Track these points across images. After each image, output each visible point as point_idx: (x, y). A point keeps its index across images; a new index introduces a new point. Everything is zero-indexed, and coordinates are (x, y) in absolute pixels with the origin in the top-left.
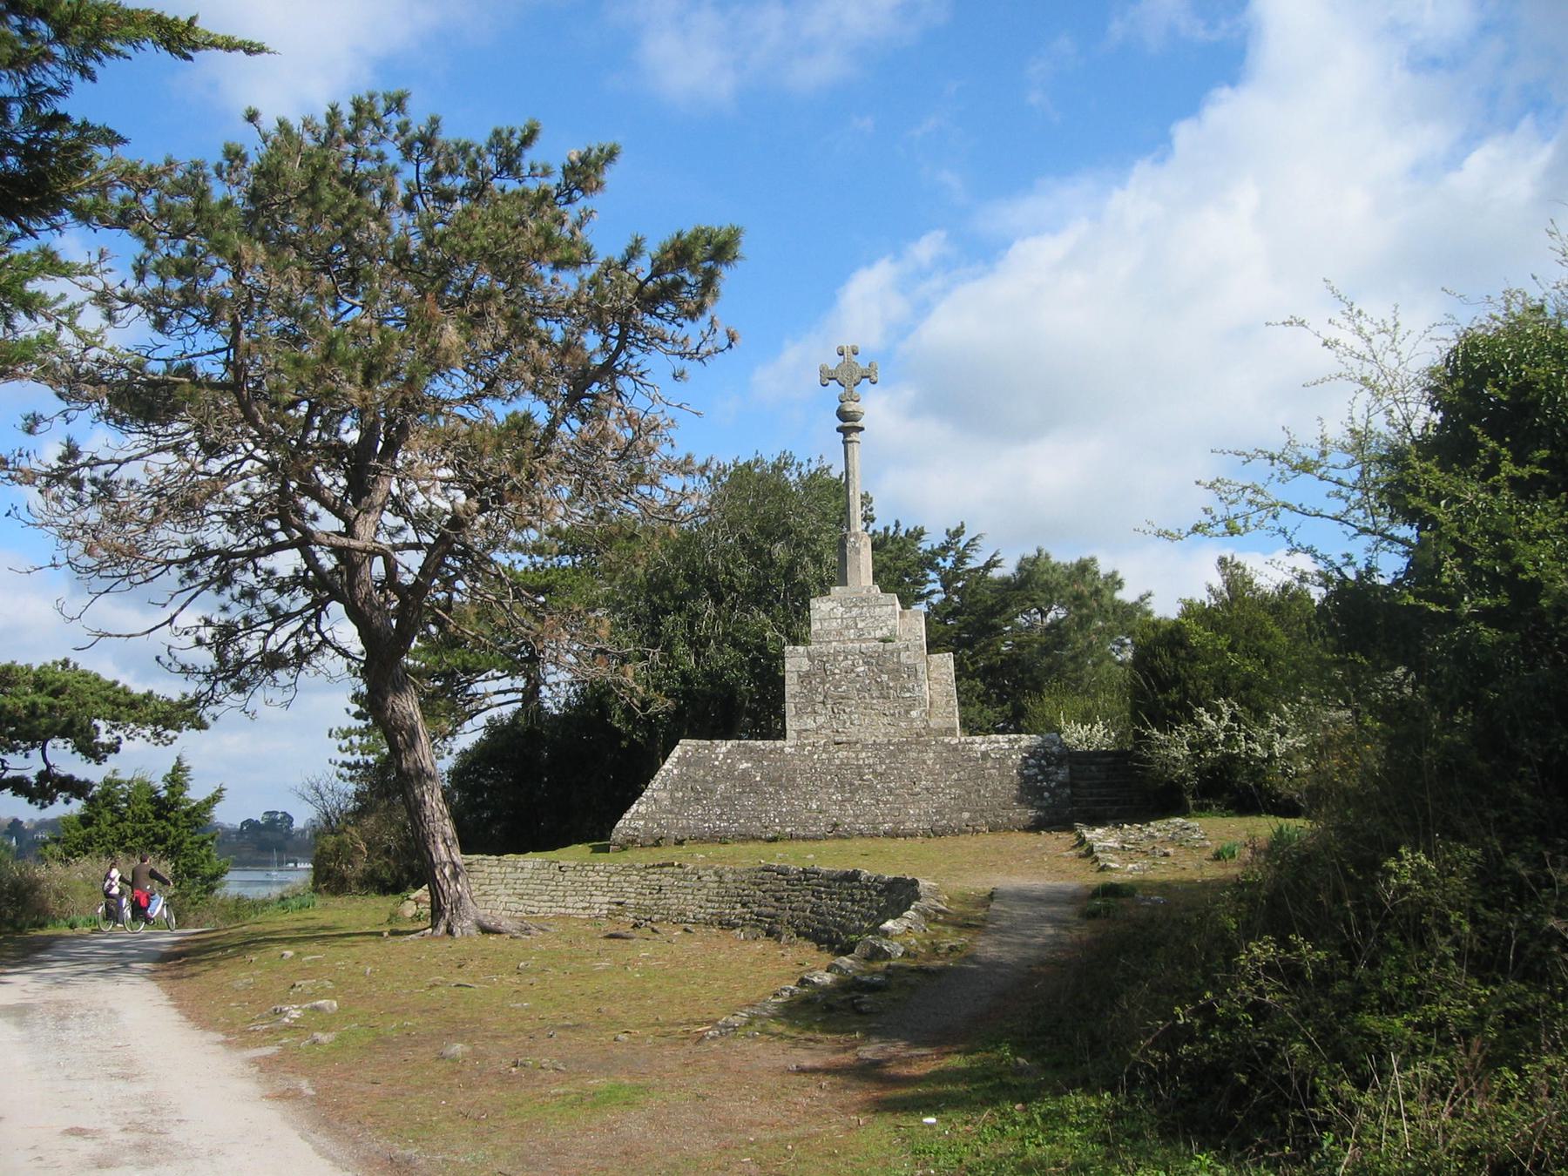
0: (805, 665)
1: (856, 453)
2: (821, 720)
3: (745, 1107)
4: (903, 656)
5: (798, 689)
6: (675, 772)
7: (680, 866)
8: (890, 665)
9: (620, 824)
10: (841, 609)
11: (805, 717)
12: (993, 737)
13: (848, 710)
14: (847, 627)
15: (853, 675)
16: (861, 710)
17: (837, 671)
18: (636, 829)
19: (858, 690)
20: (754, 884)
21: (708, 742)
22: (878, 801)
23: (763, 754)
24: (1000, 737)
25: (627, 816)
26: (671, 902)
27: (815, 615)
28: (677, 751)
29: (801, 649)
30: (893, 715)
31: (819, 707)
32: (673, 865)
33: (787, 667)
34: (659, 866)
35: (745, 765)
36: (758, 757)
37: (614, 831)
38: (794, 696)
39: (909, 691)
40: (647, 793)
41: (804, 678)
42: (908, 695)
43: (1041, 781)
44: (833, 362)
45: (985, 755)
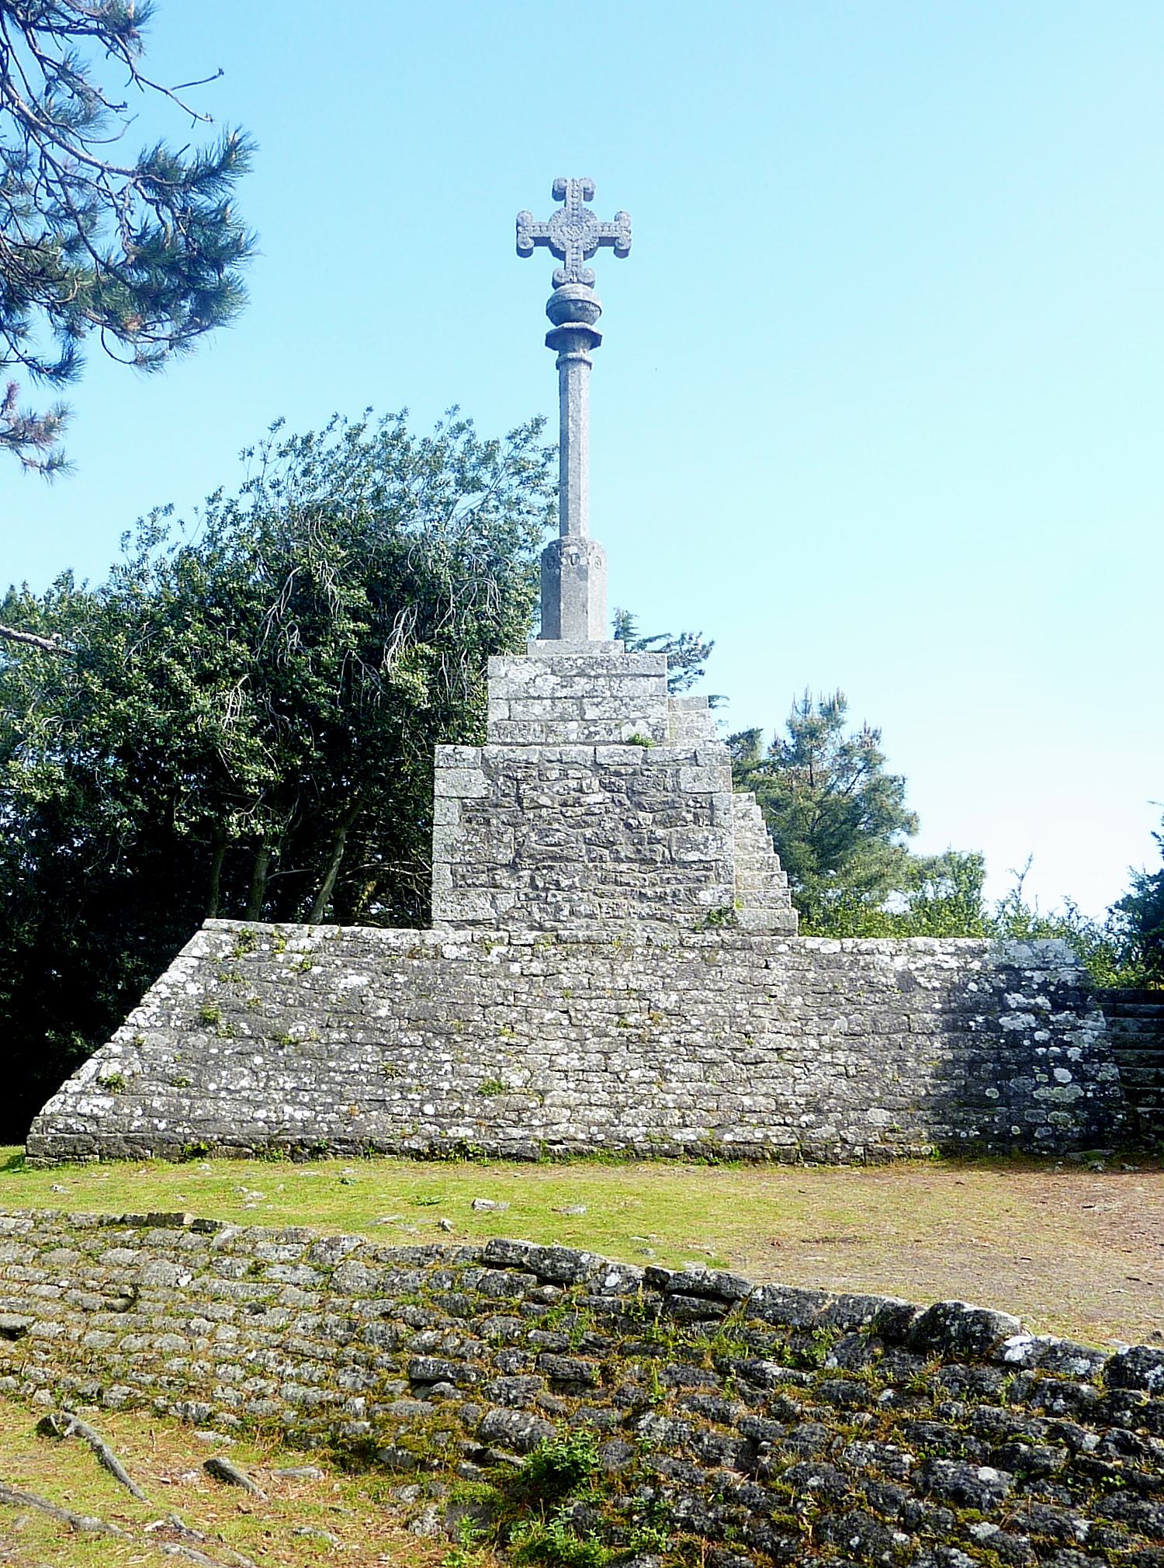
0: (478, 786)
1: (585, 385)
2: (506, 902)
3: (49, 759)
4: (687, 773)
5: (459, 833)
6: (193, 989)
7: (199, 1226)
8: (656, 796)
9: (50, 1107)
10: (553, 679)
11: (472, 893)
12: (919, 942)
13: (564, 883)
14: (563, 719)
15: (579, 810)
16: (593, 883)
17: (544, 800)
18: (95, 1119)
19: (588, 842)
20: (455, 1310)
21: (271, 928)
22: (664, 1074)
23: (388, 962)
24: (935, 943)
25: (71, 1085)
26: (162, 1342)
27: (496, 689)
28: (198, 944)
29: (469, 752)
30: (661, 898)
31: (502, 876)
32: (178, 1219)
33: (439, 787)
34: (138, 1222)
35: (357, 980)
36: (388, 962)
37: (38, 1121)
38: (452, 849)
39: (695, 847)
40: (124, 1034)
41: (475, 813)
42: (693, 856)
43: (1045, 1044)
44: (543, 211)
45: (907, 982)
